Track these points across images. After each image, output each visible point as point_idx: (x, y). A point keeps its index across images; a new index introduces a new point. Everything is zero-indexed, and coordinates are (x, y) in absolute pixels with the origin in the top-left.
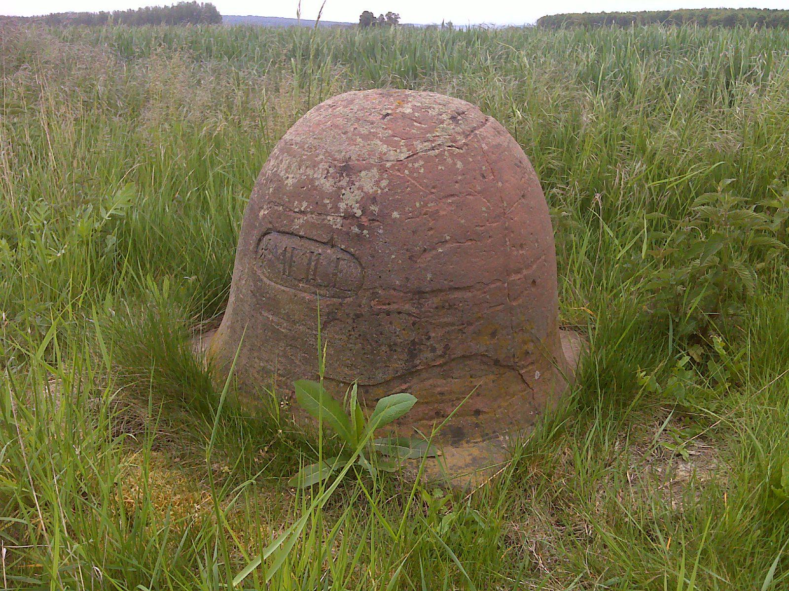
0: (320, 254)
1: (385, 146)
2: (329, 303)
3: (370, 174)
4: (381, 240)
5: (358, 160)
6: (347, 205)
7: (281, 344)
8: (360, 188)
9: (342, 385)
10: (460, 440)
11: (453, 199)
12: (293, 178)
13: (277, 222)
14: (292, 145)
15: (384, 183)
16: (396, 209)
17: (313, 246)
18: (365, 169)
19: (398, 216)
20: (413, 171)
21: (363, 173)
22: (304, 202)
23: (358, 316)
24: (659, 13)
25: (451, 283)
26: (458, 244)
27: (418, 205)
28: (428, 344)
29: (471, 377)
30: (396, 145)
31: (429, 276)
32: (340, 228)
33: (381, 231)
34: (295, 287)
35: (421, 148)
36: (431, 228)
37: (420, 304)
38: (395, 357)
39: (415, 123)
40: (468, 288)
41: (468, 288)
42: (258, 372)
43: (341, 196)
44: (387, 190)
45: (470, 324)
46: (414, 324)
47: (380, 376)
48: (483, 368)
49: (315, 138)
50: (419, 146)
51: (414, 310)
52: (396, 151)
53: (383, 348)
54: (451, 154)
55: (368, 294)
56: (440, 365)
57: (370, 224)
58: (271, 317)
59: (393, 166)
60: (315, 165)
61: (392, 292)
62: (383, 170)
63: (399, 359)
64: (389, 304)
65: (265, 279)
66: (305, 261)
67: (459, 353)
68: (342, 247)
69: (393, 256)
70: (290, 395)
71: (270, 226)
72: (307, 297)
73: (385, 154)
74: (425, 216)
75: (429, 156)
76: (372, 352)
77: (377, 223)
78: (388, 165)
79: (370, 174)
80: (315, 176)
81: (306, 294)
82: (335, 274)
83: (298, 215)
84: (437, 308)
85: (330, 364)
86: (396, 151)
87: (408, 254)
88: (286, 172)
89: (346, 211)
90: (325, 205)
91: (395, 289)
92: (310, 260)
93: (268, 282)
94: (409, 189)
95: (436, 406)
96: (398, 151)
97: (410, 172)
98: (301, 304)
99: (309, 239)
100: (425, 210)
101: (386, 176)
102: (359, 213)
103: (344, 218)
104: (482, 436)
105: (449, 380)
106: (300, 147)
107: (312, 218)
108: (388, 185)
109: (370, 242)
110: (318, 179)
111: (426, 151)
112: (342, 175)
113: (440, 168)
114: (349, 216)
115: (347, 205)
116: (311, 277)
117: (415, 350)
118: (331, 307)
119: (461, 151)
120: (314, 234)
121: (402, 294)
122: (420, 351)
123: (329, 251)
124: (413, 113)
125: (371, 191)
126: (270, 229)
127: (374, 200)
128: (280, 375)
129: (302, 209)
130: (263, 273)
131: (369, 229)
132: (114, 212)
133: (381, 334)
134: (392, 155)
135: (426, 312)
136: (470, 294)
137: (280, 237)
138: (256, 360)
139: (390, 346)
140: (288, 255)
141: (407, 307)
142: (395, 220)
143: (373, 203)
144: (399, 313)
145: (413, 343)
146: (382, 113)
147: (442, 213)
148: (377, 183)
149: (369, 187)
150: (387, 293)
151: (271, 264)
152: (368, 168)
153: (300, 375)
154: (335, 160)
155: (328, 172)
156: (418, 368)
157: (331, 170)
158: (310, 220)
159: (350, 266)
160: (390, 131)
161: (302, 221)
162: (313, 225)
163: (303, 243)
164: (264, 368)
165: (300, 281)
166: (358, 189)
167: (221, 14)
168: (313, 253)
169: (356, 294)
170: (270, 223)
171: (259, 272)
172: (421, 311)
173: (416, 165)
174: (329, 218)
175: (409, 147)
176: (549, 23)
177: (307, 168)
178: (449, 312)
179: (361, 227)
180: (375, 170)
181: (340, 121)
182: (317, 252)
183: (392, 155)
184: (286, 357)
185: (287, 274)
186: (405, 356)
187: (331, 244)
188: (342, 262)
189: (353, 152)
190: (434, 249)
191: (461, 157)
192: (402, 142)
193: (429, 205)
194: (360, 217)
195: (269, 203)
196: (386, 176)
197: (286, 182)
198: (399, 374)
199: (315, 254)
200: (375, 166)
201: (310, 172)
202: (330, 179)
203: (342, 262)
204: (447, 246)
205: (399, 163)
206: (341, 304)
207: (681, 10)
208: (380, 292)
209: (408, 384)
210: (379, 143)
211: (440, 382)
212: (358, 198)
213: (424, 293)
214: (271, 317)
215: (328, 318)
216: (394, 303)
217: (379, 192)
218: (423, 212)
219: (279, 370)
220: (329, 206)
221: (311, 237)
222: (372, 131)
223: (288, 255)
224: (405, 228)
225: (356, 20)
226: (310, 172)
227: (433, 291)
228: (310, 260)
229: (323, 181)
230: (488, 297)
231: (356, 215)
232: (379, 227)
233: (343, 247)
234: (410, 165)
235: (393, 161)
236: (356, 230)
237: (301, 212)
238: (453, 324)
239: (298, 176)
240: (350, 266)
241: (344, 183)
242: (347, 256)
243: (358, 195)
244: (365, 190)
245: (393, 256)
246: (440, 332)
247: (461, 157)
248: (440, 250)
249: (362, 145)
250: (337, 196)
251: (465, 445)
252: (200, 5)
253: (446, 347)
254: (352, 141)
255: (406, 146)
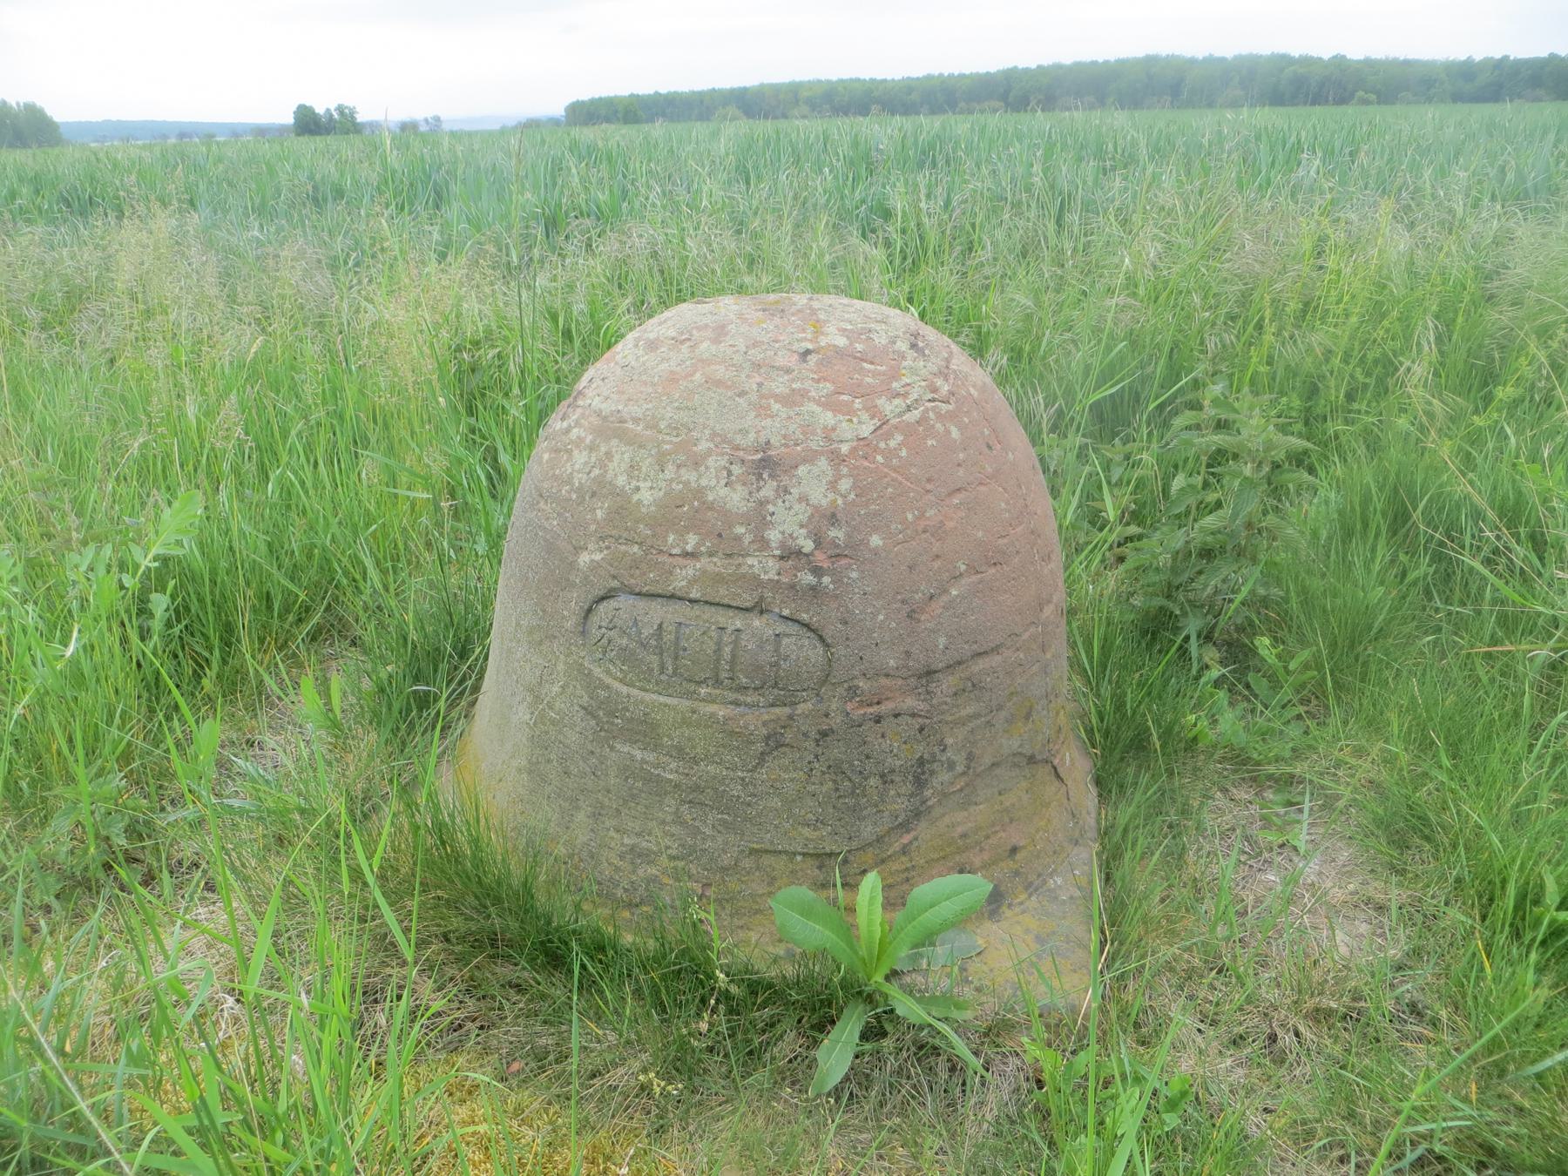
0: (738, 630)
1: (829, 414)
2: (766, 717)
3: (816, 470)
4: (856, 590)
5: (786, 445)
6: (783, 533)
7: (668, 800)
8: (803, 499)
9: (799, 858)
10: (999, 907)
11: (962, 495)
12: (651, 488)
13: (632, 576)
14: (625, 422)
15: (845, 485)
16: (875, 529)
17: (722, 617)
18: (805, 461)
19: (881, 543)
20: (890, 454)
21: (802, 470)
22: (691, 535)
23: (824, 734)
24: (732, 91)
25: (975, 647)
26: (979, 576)
27: (910, 516)
28: (944, 759)
29: (1000, 794)
30: (849, 411)
31: (942, 641)
32: (776, 578)
33: (854, 575)
34: (690, 695)
35: (892, 411)
36: (937, 556)
37: (928, 693)
38: (892, 792)
39: (865, 365)
40: (995, 650)
41: (995, 650)
42: (622, 857)
43: (769, 518)
44: (852, 496)
45: (1000, 708)
46: (921, 730)
47: (868, 831)
48: (1014, 774)
49: (678, 408)
50: (889, 407)
51: (922, 706)
52: (850, 421)
53: (873, 782)
54: (939, 416)
55: (840, 690)
56: (961, 790)
57: (833, 563)
58: (638, 754)
59: (854, 450)
60: (697, 462)
61: (883, 681)
62: (836, 459)
63: (899, 795)
64: (878, 703)
65: (616, 685)
66: (710, 647)
67: (987, 760)
68: (784, 614)
69: (881, 617)
70: (700, 892)
71: (615, 584)
72: (722, 712)
73: (834, 429)
74: (924, 536)
75: (908, 424)
76: (853, 792)
77: (844, 562)
78: (845, 448)
79: (816, 470)
80: (704, 482)
81: (716, 706)
82: (776, 664)
83: (681, 561)
84: (955, 694)
85: (776, 827)
86: (850, 421)
87: (906, 608)
88: (630, 477)
89: (783, 545)
90: (738, 538)
91: (887, 675)
92: (719, 644)
93: (625, 690)
94: (890, 490)
95: (957, 858)
96: (855, 420)
97: (885, 458)
98: (706, 727)
99: (712, 604)
100: (922, 524)
101: (845, 470)
102: (808, 546)
103: (782, 558)
104: (1026, 888)
105: (972, 809)
106: (647, 427)
107: (717, 565)
108: (854, 487)
109: (836, 597)
110: (712, 489)
111: (900, 415)
112: (760, 477)
113: (929, 443)
114: (790, 554)
115: (783, 533)
116: (724, 675)
117: (923, 773)
118: (772, 726)
119: (950, 407)
120: (723, 594)
121: (900, 682)
122: (932, 773)
123: (757, 623)
124: (851, 344)
125: (824, 502)
126: (614, 589)
127: (833, 519)
128: (672, 858)
129: (689, 548)
130: (608, 672)
131: (832, 572)
132: (162, 552)
133: (868, 757)
134: (846, 430)
135: (940, 704)
136: (998, 658)
137: (642, 604)
138: (612, 833)
139: (882, 776)
140: (668, 638)
141: (910, 702)
142: (876, 552)
143: (833, 524)
144: (896, 716)
145: (921, 762)
146: (794, 348)
147: (950, 524)
148: (833, 486)
149: (820, 496)
150: (875, 684)
151: (626, 656)
152: (810, 458)
153: (716, 854)
154: (737, 448)
155: (730, 473)
156: (930, 803)
157: (737, 470)
158: (710, 568)
159: (802, 646)
160: (828, 385)
161: (691, 572)
162: (719, 579)
163: (698, 613)
164: (633, 848)
165: (699, 683)
166: (800, 500)
167: (57, 119)
168: (723, 629)
169: (818, 695)
170: (614, 577)
171: (597, 671)
172: (932, 706)
173: (892, 444)
174: (750, 561)
175: (874, 412)
176: (587, 113)
177: (679, 466)
178: (972, 696)
179: (817, 571)
180: (823, 463)
181: (720, 372)
182: (733, 628)
183: (846, 430)
184: (683, 823)
185: (670, 671)
186: (907, 788)
187: (760, 608)
188: (785, 641)
189: (774, 428)
190: (946, 591)
191: (952, 417)
192: (858, 403)
193: (928, 515)
194: (811, 554)
195: (602, 539)
196: (845, 470)
197: (636, 497)
198: (900, 820)
199: (729, 631)
200: (822, 453)
201: (689, 475)
202: (739, 487)
203: (785, 641)
204: (963, 582)
205: (862, 443)
206: (791, 717)
207: (762, 85)
208: (861, 684)
209: (913, 834)
210: (818, 409)
211: (960, 816)
212: (803, 518)
213: (936, 672)
214: (638, 754)
215: (767, 744)
216: (887, 699)
217: (840, 501)
218: (920, 529)
219: (668, 848)
220: (748, 539)
221: (717, 600)
222: (794, 386)
223: (668, 638)
224: (895, 562)
225: (289, 119)
226: (689, 475)
227: (949, 667)
228: (719, 644)
229: (723, 492)
230: (1022, 656)
231: (805, 550)
232: (849, 567)
233: (786, 612)
234: (882, 445)
235: (852, 440)
236: (808, 578)
237: (686, 555)
238: (977, 716)
239: (663, 484)
240: (802, 646)
241: (768, 491)
242: (793, 628)
243: (802, 512)
244: (814, 501)
245: (881, 617)
246: (961, 733)
247: (952, 417)
248: (954, 593)
249: (784, 416)
250: (760, 519)
251: (1008, 913)
252: (14, 105)
253: (970, 757)
254: (762, 410)
255: (866, 409)
